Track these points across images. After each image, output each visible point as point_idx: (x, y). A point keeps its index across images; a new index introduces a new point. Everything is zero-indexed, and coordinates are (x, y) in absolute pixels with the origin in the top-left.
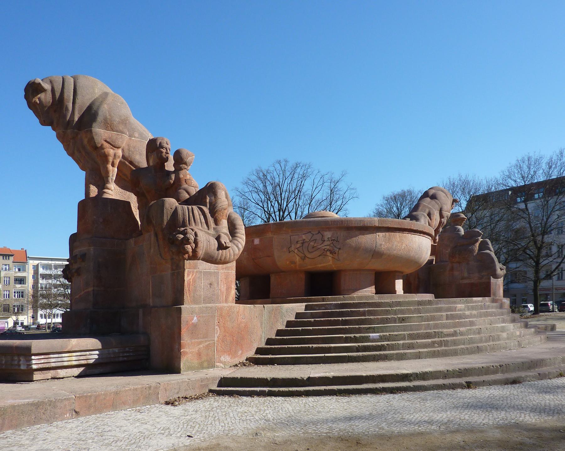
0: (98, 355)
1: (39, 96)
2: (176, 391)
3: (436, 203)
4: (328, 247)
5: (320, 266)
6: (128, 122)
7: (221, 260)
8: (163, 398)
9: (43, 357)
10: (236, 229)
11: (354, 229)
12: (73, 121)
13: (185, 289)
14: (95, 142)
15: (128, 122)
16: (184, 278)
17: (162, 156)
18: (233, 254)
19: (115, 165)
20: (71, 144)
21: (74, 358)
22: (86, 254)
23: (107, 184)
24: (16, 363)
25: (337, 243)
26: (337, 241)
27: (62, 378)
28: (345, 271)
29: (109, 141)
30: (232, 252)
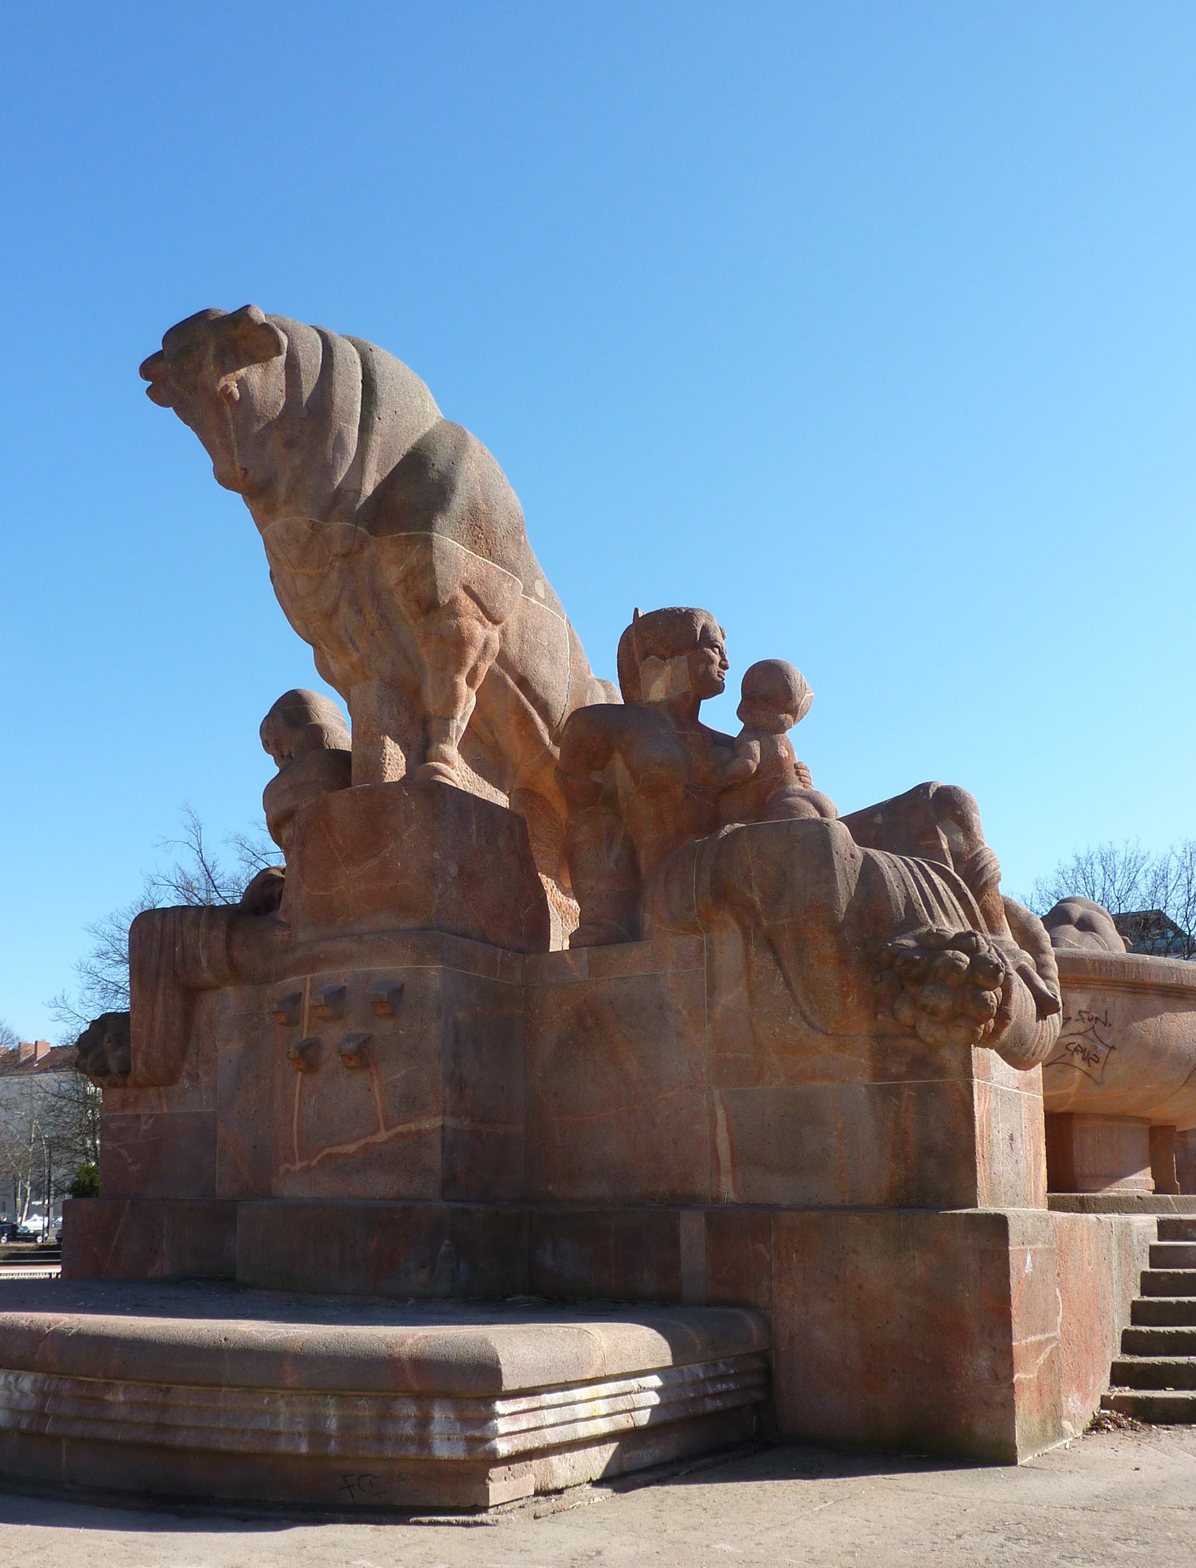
0: (658, 1390)
1: (242, 372)
3: (1098, 941)
4: (1079, 1040)
11: (1151, 991)
12: (358, 492)
17: (708, 673)
20: (334, 576)
22: (403, 986)
23: (442, 742)
24: (408, 1429)
25: (1106, 1028)
26: (1105, 1025)
28: (1082, 1116)
29: (477, 591)
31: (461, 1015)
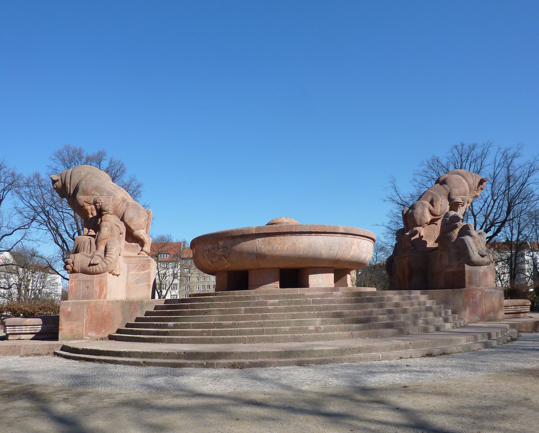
1: (56, 184)
2: (32, 350)
4: (222, 253)
5: (226, 267)
6: (98, 188)
8: (22, 352)
9: (12, 327)
21: (28, 329)
27: (24, 339)
30: (101, 267)
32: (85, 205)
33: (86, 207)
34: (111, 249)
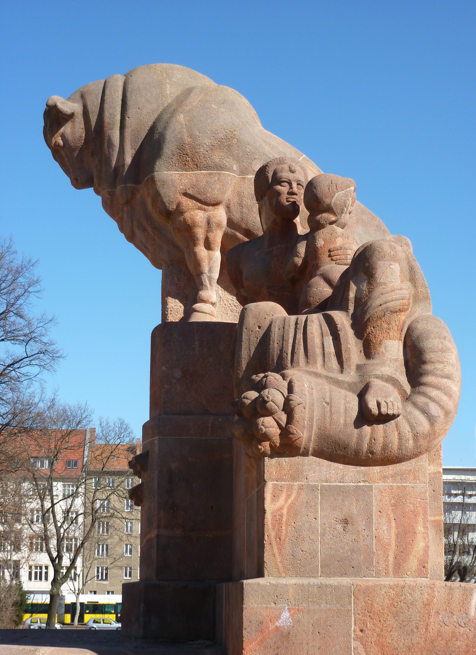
1: (62, 130)
6: (235, 141)
7: (372, 453)
10: (424, 362)
12: (123, 165)
13: (266, 534)
14: (163, 203)
15: (235, 141)
16: (263, 503)
17: (279, 203)
18: (409, 435)
19: (213, 246)
20: (125, 216)
23: (201, 290)
30: (406, 428)
31: (174, 466)
32: (184, 207)
33: (187, 215)
34: (443, 351)
